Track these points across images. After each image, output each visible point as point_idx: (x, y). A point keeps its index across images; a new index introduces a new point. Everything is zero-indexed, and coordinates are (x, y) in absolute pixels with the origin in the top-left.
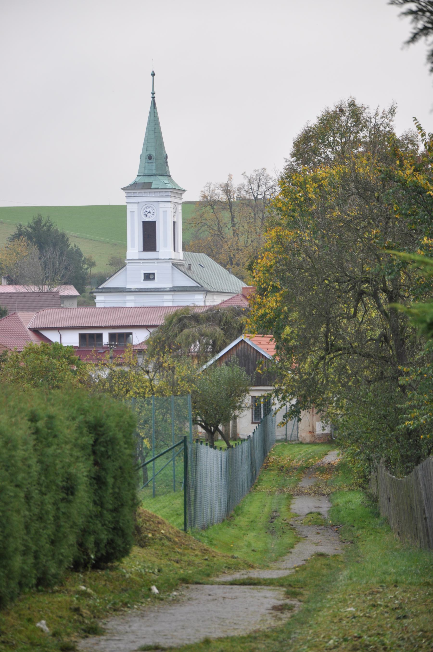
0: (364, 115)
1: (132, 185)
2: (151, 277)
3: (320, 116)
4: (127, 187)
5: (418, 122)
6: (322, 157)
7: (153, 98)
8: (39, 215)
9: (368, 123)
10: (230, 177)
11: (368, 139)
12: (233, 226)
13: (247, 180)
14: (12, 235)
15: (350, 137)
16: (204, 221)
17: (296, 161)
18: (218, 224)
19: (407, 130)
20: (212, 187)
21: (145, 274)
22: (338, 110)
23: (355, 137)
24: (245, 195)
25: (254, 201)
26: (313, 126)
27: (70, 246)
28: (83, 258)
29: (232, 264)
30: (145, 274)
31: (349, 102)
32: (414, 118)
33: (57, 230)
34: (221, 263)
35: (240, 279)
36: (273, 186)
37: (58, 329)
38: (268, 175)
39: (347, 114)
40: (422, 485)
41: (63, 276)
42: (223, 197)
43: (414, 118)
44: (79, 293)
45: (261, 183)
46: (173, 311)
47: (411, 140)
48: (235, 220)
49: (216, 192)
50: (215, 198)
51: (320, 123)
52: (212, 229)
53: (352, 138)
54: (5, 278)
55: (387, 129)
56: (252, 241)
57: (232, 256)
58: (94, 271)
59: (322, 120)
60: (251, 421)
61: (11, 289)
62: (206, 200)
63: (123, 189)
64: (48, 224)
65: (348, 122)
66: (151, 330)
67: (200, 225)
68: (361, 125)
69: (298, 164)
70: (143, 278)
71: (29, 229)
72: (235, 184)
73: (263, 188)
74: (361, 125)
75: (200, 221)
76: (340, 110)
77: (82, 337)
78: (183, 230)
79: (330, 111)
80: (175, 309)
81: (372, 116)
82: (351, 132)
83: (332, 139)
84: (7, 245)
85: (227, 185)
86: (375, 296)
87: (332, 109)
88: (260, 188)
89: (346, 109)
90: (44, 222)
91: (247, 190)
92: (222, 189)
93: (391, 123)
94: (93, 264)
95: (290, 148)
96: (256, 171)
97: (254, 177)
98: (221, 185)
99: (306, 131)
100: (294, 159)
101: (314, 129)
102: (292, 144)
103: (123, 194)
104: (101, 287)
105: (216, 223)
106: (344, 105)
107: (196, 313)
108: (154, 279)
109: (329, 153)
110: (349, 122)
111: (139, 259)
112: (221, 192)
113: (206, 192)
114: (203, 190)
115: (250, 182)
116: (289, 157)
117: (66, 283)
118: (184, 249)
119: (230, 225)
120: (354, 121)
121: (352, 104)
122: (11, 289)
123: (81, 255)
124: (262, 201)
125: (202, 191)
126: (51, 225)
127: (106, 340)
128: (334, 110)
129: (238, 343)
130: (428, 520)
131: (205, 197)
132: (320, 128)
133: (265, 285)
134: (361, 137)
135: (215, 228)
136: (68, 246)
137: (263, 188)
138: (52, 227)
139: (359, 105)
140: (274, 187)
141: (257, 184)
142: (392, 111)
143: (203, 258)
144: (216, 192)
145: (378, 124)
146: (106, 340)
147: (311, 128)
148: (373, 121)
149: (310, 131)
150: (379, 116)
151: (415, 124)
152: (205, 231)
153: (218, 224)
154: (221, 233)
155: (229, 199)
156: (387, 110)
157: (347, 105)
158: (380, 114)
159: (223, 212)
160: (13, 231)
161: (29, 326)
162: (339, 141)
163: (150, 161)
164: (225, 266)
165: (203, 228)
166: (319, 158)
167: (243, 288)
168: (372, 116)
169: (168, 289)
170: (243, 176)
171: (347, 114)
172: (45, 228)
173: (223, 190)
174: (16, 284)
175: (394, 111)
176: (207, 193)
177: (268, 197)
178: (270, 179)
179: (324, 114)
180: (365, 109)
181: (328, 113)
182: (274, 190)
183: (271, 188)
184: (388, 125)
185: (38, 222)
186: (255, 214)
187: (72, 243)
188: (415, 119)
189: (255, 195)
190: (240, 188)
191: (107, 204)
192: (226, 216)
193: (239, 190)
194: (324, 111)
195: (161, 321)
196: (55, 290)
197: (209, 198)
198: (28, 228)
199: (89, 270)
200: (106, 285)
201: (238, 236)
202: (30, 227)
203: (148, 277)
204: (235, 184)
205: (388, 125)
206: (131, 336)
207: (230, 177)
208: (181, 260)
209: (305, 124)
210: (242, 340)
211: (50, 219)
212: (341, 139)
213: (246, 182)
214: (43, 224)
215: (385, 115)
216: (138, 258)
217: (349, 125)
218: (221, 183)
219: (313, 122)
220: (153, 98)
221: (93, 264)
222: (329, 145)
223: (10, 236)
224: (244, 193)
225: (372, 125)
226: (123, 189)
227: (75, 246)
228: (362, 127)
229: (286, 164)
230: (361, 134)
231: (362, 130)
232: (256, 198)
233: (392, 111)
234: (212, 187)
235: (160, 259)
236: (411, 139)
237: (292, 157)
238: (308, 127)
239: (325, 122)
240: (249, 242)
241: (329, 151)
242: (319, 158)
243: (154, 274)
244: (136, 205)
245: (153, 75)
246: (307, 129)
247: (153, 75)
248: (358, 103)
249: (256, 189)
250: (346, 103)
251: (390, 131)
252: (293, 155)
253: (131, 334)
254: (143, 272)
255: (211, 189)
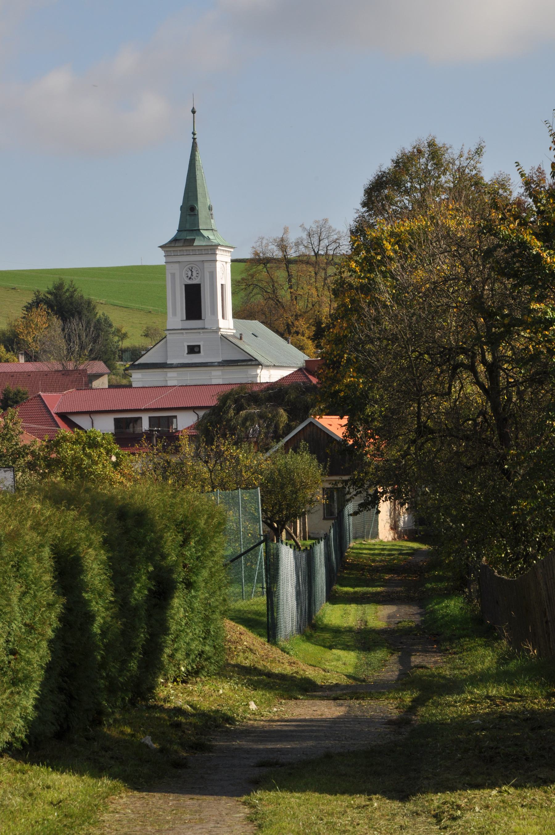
0: (446, 156)
1: (171, 242)
2: (196, 349)
3: (395, 158)
4: (166, 244)
5: (518, 170)
6: (398, 207)
7: (194, 139)
8: (60, 279)
9: (451, 165)
10: (286, 230)
11: (452, 185)
12: (291, 287)
13: (306, 233)
14: (29, 304)
15: (430, 181)
16: (255, 283)
17: (368, 211)
18: (273, 286)
19: (497, 173)
20: (265, 242)
21: (188, 346)
22: (415, 150)
23: (437, 182)
24: (304, 251)
25: (315, 257)
26: (387, 171)
27: (98, 315)
28: (113, 329)
29: (290, 333)
30: (188, 346)
31: (429, 140)
32: (516, 163)
33: (82, 297)
34: (277, 332)
35: (300, 350)
36: (337, 239)
37: (90, 413)
38: (330, 227)
39: (426, 155)
40: (542, 584)
41: (91, 350)
42: (278, 254)
43: (516, 163)
44: (110, 370)
45: (323, 236)
46: (227, 389)
47: (503, 185)
48: (293, 281)
49: (270, 248)
50: (269, 255)
51: (395, 167)
52: (266, 292)
53: (433, 183)
54: (22, 354)
55: (474, 172)
56: (313, 306)
57: (290, 323)
58: (126, 344)
59: (397, 163)
60: (323, 517)
61: (31, 367)
62: (257, 257)
63: (160, 247)
64: (71, 290)
65: (427, 165)
66: (201, 413)
67: (251, 287)
68: (443, 168)
69: (370, 215)
70: (186, 351)
71: (49, 296)
72: (292, 238)
73: (325, 242)
74: (443, 168)
75: (250, 283)
76: (417, 150)
77: (116, 421)
78: (233, 293)
79: (407, 152)
80: (230, 387)
81: (456, 157)
82: (433, 177)
83: (409, 185)
84: (24, 315)
85: (282, 240)
86: (472, 368)
87: (408, 149)
88: (321, 242)
89: (426, 150)
90: (66, 287)
91: (306, 245)
92: (276, 244)
93: (478, 165)
94: (124, 336)
95: (360, 196)
96: (316, 222)
97: (314, 229)
98: (275, 240)
99: (379, 177)
100: (365, 209)
101: (388, 173)
102: (362, 193)
103: (162, 253)
104: (137, 363)
105: (271, 284)
106: (423, 145)
107: (255, 392)
108: (199, 352)
109: (406, 202)
110: (430, 164)
111: (181, 329)
112: (275, 248)
113: (258, 248)
114: (254, 245)
115: (309, 235)
116: (359, 207)
117: (94, 359)
118: (236, 315)
119: (287, 286)
120: (434, 164)
121: (431, 144)
122: (31, 367)
123: (111, 326)
124: (324, 257)
125: (253, 247)
126: (75, 290)
127: (145, 426)
128: (411, 151)
129: (306, 426)
130: (550, 624)
131: (256, 254)
132: (395, 172)
133: (338, 357)
134: (443, 181)
135: (269, 291)
136: (96, 315)
137: (325, 242)
138: (76, 293)
139: (440, 145)
140: (338, 241)
141: (317, 238)
142: (479, 152)
143: (256, 325)
144: (270, 248)
145: (463, 167)
146: (145, 426)
147: (384, 172)
148: (457, 162)
149: (383, 176)
150: (464, 157)
151: (518, 170)
152: (258, 294)
153: (273, 286)
154: (276, 297)
155: (285, 256)
156: (473, 149)
157: (426, 144)
158: (466, 155)
159: (278, 271)
160: (30, 298)
161: (56, 411)
162: (418, 187)
163: (192, 213)
164: (282, 335)
165: (255, 291)
166: (394, 208)
167: (306, 361)
168: (456, 157)
169: (216, 364)
170: (300, 229)
171: (426, 155)
172: (67, 294)
173: (278, 246)
174: (35, 361)
175: (481, 151)
176: (259, 250)
177: (331, 253)
178: (334, 231)
179: (400, 156)
180: (447, 149)
181: (404, 155)
182: (338, 245)
183: (335, 242)
184: (474, 168)
185: (59, 287)
186: (316, 274)
187: (100, 312)
188: (518, 164)
189: (316, 250)
190: (298, 242)
191: (139, 264)
192: (281, 275)
193: (297, 244)
194: (399, 153)
195: (213, 402)
196: (81, 367)
197: (261, 255)
198: (47, 295)
199: (120, 343)
200: (141, 361)
201: (296, 299)
202: (50, 293)
203: (193, 350)
204: (292, 238)
205: (474, 168)
206: (174, 420)
207: (286, 230)
208: (231, 329)
209: (378, 168)
210: (311, 422)
211: (73, 284)
212: (420, 185)
213: (304, 235)
214: (64, 290)
215: (471, 156)
216: (180, 328)
217: (429, 168)
218: (275, 238)
219: (387, 165)
220: (194, 139)
221: (124, 336)
222: (407, 192)
223: (26, 304)
224: (303, 249)
225: (456, 167)
226: (160, 247)
227: (103, 314)
228: (444, 170)
229: (357, 215)
230: (443, 179)
231: (444, 173)
232: (317, 255)
233: (479, 152)
234: (265, 242)
235: (206, 329)
236: (502, 182)
237: (363, 207)
238: (381, 172)
239: (401, 165)
240: (310, 306)
241: (406, 200)
242: (394, 208)
243: (199, 346)
244: (177, 265)
245: (194, 112)
246: (380, 173)
247: (194, 112)
248: (439, 142)
249: (316, 243)
250: (425, 142)
251: (477, 174)
252: (364, 205)
253: (175, 417)
254: (186, 344)
255: (264, 244)
